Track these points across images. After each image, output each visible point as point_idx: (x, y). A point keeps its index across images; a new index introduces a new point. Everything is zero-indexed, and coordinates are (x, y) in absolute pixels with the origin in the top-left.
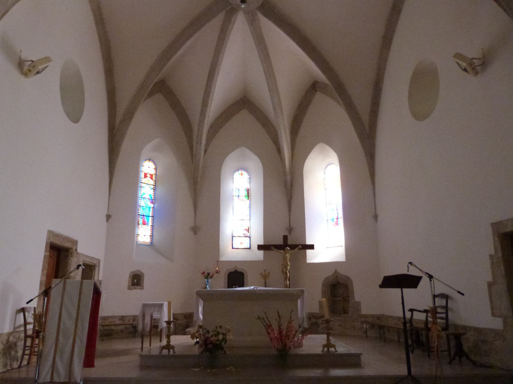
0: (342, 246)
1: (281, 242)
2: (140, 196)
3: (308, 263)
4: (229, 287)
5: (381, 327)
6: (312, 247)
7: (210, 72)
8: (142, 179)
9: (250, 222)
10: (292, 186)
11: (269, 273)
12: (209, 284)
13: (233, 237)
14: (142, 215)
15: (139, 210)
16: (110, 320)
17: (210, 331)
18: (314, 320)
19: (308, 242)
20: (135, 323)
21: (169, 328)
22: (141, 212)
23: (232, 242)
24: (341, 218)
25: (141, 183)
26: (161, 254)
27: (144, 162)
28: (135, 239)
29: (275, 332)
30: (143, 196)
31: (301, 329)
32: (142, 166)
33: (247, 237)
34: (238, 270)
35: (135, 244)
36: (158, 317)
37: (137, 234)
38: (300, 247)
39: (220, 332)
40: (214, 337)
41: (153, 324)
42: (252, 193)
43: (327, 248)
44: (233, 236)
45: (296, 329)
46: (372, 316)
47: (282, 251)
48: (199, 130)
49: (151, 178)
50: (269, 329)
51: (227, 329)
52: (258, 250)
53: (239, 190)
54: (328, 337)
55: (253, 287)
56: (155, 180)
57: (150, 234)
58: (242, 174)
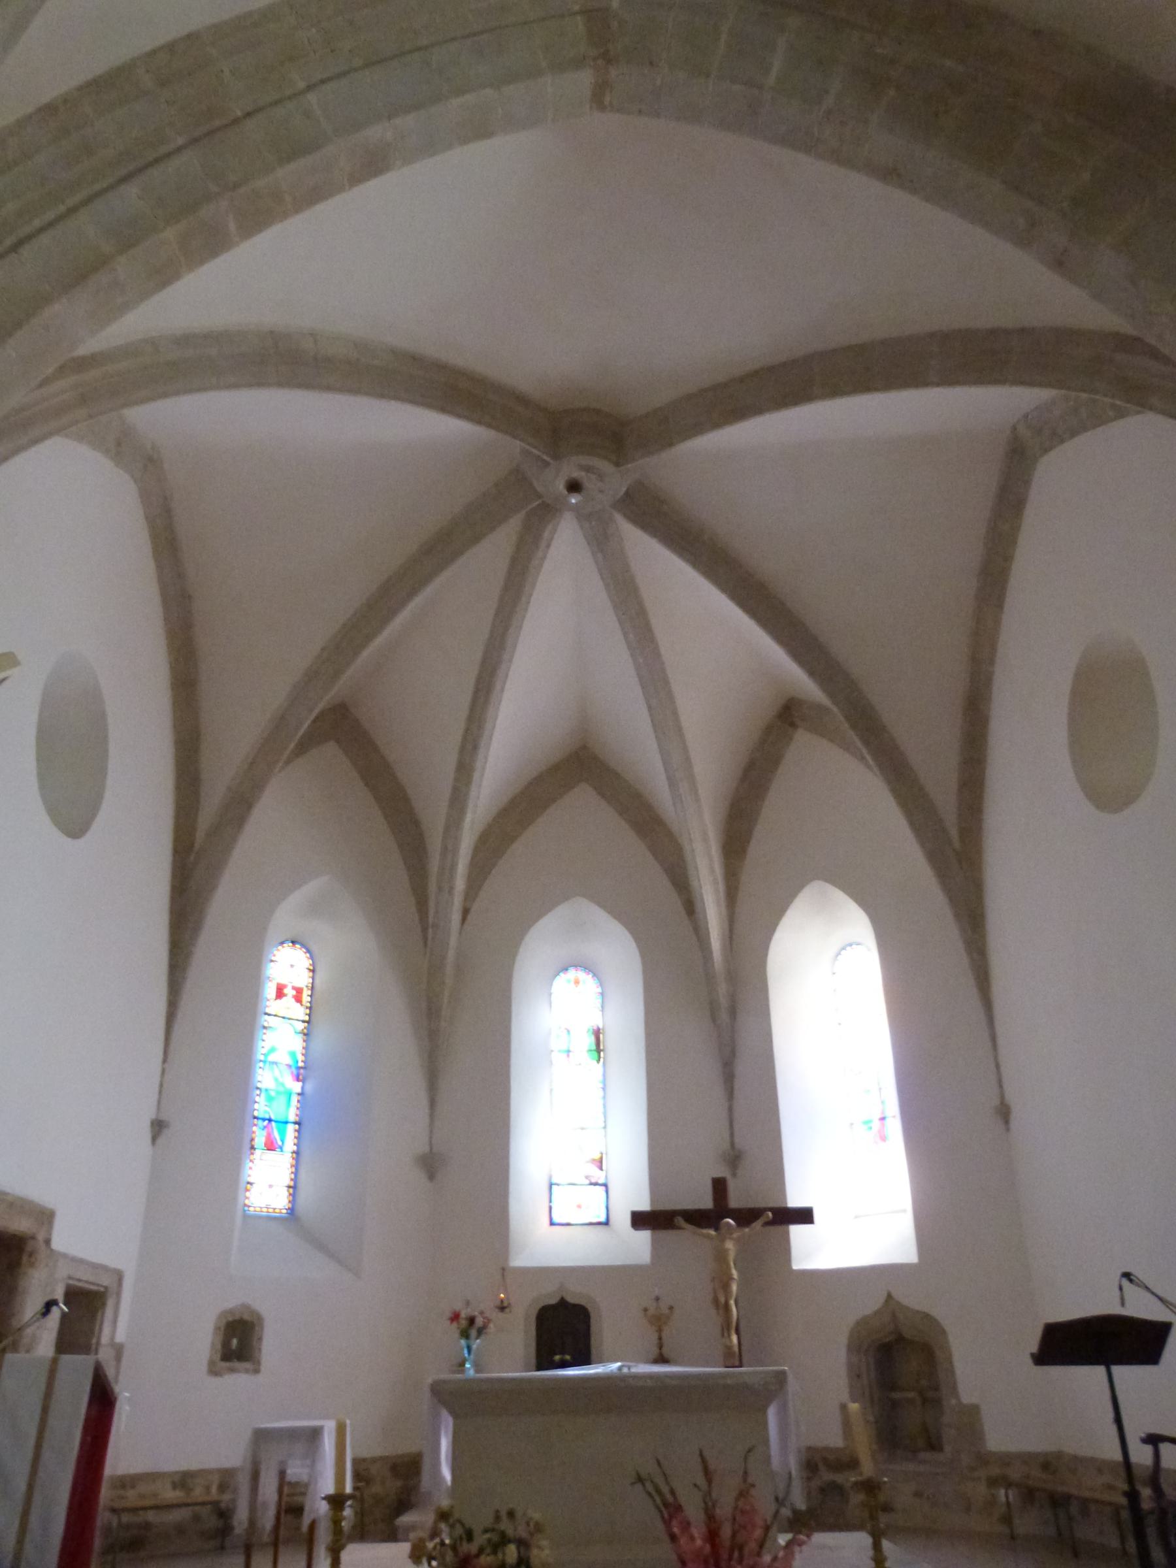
0: (904, 1211)
1: (706, 1202)
2: (262, 1058)
3: (796, 1270)
4: (540, 1367)
5: (1058, 1501)
6: (805, 1216)
7: (479, 680)
8: (268, 1003)
9: (605, 1136)
10: (733, 1012)
11: (671, 1308)
12: (472, 1356)
13: (551, 1185)
14: (264, 1120)
15: (256, 1102)
16: (142, 1488)
17: (477, 1530)
18: (827, 1476)
19: (795, 1200)
20: (226, 1497)
21: (336, 1522)
22: (261, 1107)
23: (550, 1201)
24: (894, 1117)
25: (266, 1014)
26: (319, 1245)
27: (278, 950)
28: (241, 1201)
29: (696, 1535)
30: (271, 1058)
31: (786, 1512)
32: (272, 961)
33: (596, 1184)
34: (571, 1299)
35: (239, 1213)
36: (305, 1478)
37: (248, 1183)
38: (768, 1215)
39: (510, 1532)
40: (488, 1555)
41: (285, 1499)
42: (610, 1041)
43: (856, 1217)
44: (554, 1181)
45: (766, 1520)
46: (1026, 1458)
47: (712, 1232)
48: (445, 850)
49: (298, 999)
50: (674, 1523)
51: (532, 1525)
52: (632, 1230)
53: (568, 1031)
54: (877, 1546)
55: (619, 1364)
56: (309, 1005)
57: (288, 1182)
58: (577, 982)
